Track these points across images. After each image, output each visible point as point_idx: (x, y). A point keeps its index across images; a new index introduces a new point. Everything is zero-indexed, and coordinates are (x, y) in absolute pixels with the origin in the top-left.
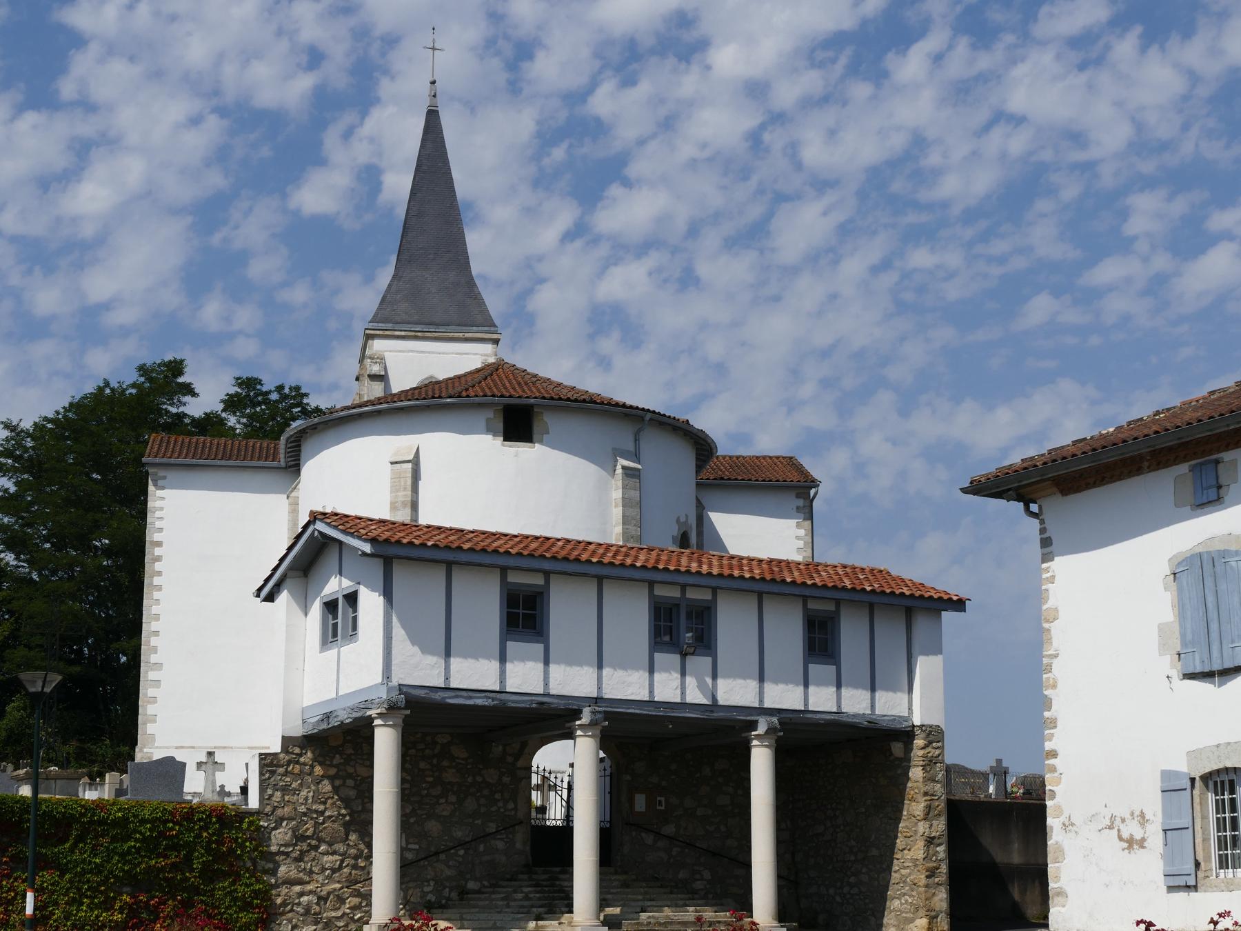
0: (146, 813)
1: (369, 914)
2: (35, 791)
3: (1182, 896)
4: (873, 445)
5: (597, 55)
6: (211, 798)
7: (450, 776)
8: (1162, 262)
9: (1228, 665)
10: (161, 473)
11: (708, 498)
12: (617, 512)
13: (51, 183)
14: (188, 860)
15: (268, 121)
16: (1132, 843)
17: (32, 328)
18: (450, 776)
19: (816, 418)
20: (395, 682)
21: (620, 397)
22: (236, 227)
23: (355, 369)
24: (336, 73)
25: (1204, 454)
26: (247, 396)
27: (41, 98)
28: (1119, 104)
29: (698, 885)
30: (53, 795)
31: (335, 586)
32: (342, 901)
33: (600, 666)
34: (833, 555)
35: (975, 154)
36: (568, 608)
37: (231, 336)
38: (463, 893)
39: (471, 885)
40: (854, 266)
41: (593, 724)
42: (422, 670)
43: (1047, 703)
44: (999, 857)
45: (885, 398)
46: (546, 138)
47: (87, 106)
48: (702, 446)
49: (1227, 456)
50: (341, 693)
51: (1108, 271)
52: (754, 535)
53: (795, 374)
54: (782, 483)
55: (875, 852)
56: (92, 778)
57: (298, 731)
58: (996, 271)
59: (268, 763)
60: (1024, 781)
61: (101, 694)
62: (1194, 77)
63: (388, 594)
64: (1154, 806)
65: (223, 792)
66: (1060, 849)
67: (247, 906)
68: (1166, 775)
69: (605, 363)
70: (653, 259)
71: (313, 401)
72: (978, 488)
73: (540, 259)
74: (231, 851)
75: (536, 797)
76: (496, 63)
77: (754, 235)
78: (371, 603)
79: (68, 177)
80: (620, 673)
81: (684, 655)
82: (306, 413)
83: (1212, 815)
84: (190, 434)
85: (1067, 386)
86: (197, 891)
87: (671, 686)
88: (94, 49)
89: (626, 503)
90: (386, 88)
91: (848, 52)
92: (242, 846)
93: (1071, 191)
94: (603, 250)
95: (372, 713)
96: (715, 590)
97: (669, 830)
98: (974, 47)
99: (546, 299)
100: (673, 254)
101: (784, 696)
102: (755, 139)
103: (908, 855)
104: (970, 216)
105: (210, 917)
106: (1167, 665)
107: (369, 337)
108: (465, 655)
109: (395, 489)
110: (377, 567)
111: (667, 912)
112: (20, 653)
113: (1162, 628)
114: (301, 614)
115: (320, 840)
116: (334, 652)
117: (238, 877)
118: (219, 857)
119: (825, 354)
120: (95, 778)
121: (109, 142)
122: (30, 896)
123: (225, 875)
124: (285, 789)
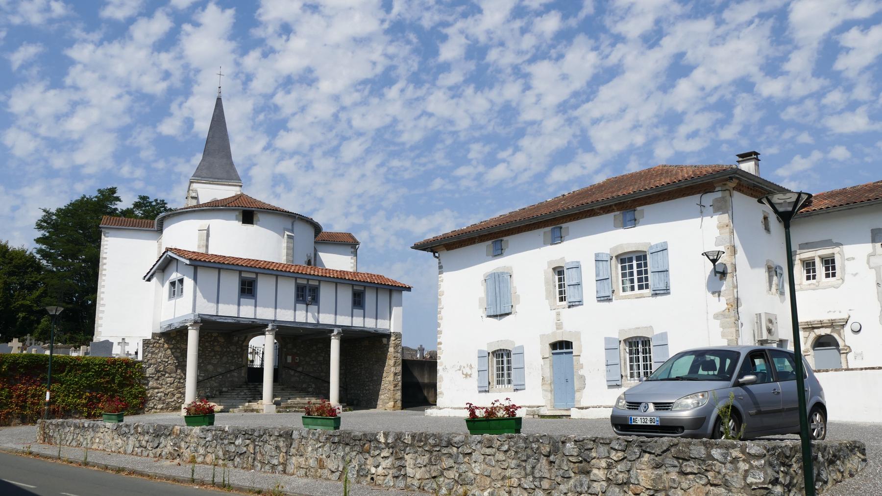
0: (97, 362)
1: (184, 400)
2: (51, 353)
3: (484, 394)
4: (377, 230)
5: (276, 81)
6: (123, 356)
7: (217, 348)
8: (481, 168)
9: (503, 313)
10: (107, 231)
11: (319, 247)
12: (284, 252)
13: (59, 117)
14: (113, 380)
15: (148, 98)
16: (466, 375)
17: (51, 173)
18: (217, 348)
19: (357, 220)
20: (197, 313)
21: (286, 209)
22: (135, 138)
23: (185, 194)
24: (176, 80)
25: (497, 237)
26: (143, 202)
27: (57, 84)
28: (466, 111)
29: (310, 390)
30: (59, 354)
31: (175, 276)
32: (173, 395)
33: (276, 308)
34: (362, 270)
35: (415, 126)
36: (264, 286)
37: (134, 180)
38: (221, 392)
39: (224, 389)
40: (371, 165)
41: (272, 330)
42: (208, 309)
43: (439, 325)
44: (420, 380)
45: (382, 213)
46: (257, 111)
47: (76, 88)
48: (317, 228)
49: (505, 239)
50: (816, 374)
51: (462, 171)
52: (335, 261)
53: (349, 203)
54: (347, 243)
55: (375, 378)
56: (76, 348)
57: (158, 331)
58: (422, 169)
59: (146, 343)
60: (430, 353)
61: (80, 318)
62: (491, 101)
63: (195, 279)
64: (475, 362)
65: (128, 354)
66: (442, 377)
67: (136, 397)
68: (480, 351)
69: (277, 196)
70: (296, 158)
71: (168, 206)
72: (417, 247)
73: (255, 156)
74: (131, 376)
75: (250, 357)
76: (238, 81)
77: (334, 152)
78: (189, 283)
79: (69, 115)
80: (283, 311)
81: (307, 305)
82: (166, 210)
83: (495, 366)
84: (120, 216)
85: (447, 212)
86: (116, 391)
87: (302, 316)
88: (79, 67)
89: (288, 248)
90: (196, 89)
91: (369, 86)
92: (135, 374)
93: (449, 142)
94: (277, 154)
95: (188, 324)
96: (320, 281)
97: (300, 369)
98: (415, 87)
99: (255, 171)
100: (305, 158)
101: (344, 321)
102: (336, 116)
103: (387, 379)
104: (413, 148)
105: (121, 401)
106: (482, 313)
107: (191, 182)
108: (224, 303)
109: (199, 240)
110: (192, 269)
111: (298, 399)
112: (47, 299)
113: (480, 299)
114: (160, 286)
115: (166, 372)
116: (173, 301)
117: (133, 386)
118: (125, 378)
119: (360, 196)
120: (77, 348)
121: (84, 103)
122: (48, 393)
123: (128, 385)
124: (152, 353)
